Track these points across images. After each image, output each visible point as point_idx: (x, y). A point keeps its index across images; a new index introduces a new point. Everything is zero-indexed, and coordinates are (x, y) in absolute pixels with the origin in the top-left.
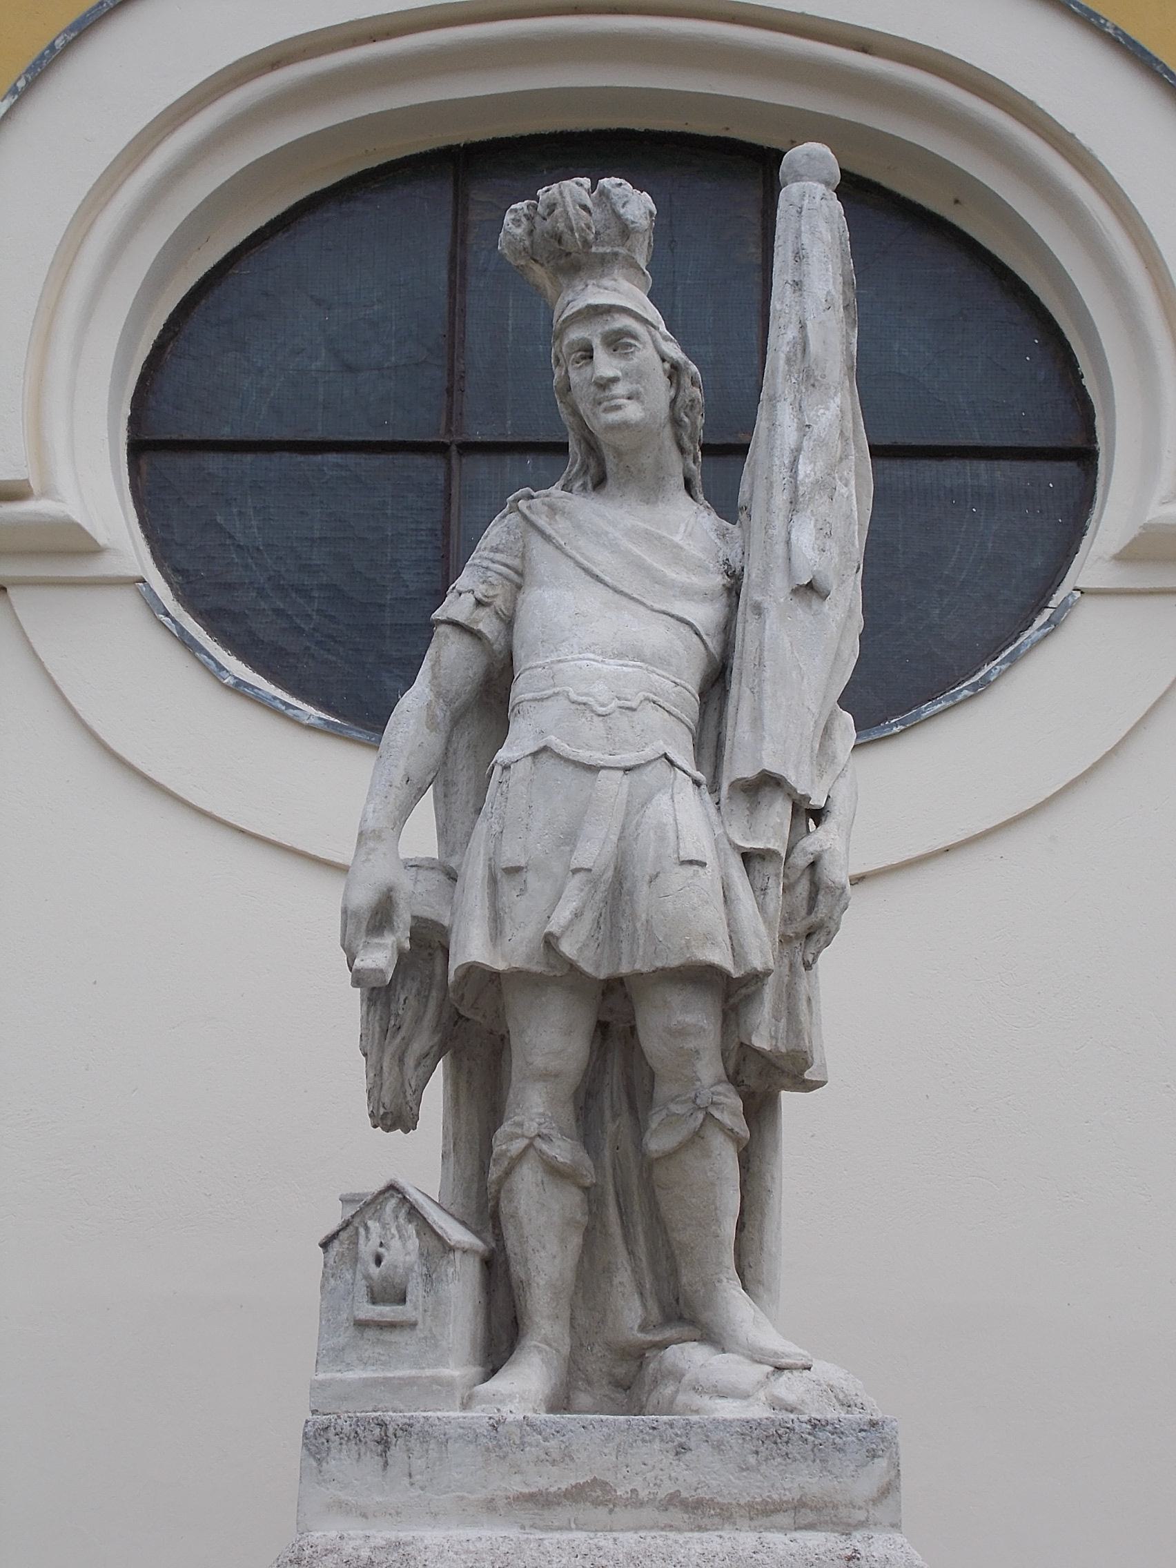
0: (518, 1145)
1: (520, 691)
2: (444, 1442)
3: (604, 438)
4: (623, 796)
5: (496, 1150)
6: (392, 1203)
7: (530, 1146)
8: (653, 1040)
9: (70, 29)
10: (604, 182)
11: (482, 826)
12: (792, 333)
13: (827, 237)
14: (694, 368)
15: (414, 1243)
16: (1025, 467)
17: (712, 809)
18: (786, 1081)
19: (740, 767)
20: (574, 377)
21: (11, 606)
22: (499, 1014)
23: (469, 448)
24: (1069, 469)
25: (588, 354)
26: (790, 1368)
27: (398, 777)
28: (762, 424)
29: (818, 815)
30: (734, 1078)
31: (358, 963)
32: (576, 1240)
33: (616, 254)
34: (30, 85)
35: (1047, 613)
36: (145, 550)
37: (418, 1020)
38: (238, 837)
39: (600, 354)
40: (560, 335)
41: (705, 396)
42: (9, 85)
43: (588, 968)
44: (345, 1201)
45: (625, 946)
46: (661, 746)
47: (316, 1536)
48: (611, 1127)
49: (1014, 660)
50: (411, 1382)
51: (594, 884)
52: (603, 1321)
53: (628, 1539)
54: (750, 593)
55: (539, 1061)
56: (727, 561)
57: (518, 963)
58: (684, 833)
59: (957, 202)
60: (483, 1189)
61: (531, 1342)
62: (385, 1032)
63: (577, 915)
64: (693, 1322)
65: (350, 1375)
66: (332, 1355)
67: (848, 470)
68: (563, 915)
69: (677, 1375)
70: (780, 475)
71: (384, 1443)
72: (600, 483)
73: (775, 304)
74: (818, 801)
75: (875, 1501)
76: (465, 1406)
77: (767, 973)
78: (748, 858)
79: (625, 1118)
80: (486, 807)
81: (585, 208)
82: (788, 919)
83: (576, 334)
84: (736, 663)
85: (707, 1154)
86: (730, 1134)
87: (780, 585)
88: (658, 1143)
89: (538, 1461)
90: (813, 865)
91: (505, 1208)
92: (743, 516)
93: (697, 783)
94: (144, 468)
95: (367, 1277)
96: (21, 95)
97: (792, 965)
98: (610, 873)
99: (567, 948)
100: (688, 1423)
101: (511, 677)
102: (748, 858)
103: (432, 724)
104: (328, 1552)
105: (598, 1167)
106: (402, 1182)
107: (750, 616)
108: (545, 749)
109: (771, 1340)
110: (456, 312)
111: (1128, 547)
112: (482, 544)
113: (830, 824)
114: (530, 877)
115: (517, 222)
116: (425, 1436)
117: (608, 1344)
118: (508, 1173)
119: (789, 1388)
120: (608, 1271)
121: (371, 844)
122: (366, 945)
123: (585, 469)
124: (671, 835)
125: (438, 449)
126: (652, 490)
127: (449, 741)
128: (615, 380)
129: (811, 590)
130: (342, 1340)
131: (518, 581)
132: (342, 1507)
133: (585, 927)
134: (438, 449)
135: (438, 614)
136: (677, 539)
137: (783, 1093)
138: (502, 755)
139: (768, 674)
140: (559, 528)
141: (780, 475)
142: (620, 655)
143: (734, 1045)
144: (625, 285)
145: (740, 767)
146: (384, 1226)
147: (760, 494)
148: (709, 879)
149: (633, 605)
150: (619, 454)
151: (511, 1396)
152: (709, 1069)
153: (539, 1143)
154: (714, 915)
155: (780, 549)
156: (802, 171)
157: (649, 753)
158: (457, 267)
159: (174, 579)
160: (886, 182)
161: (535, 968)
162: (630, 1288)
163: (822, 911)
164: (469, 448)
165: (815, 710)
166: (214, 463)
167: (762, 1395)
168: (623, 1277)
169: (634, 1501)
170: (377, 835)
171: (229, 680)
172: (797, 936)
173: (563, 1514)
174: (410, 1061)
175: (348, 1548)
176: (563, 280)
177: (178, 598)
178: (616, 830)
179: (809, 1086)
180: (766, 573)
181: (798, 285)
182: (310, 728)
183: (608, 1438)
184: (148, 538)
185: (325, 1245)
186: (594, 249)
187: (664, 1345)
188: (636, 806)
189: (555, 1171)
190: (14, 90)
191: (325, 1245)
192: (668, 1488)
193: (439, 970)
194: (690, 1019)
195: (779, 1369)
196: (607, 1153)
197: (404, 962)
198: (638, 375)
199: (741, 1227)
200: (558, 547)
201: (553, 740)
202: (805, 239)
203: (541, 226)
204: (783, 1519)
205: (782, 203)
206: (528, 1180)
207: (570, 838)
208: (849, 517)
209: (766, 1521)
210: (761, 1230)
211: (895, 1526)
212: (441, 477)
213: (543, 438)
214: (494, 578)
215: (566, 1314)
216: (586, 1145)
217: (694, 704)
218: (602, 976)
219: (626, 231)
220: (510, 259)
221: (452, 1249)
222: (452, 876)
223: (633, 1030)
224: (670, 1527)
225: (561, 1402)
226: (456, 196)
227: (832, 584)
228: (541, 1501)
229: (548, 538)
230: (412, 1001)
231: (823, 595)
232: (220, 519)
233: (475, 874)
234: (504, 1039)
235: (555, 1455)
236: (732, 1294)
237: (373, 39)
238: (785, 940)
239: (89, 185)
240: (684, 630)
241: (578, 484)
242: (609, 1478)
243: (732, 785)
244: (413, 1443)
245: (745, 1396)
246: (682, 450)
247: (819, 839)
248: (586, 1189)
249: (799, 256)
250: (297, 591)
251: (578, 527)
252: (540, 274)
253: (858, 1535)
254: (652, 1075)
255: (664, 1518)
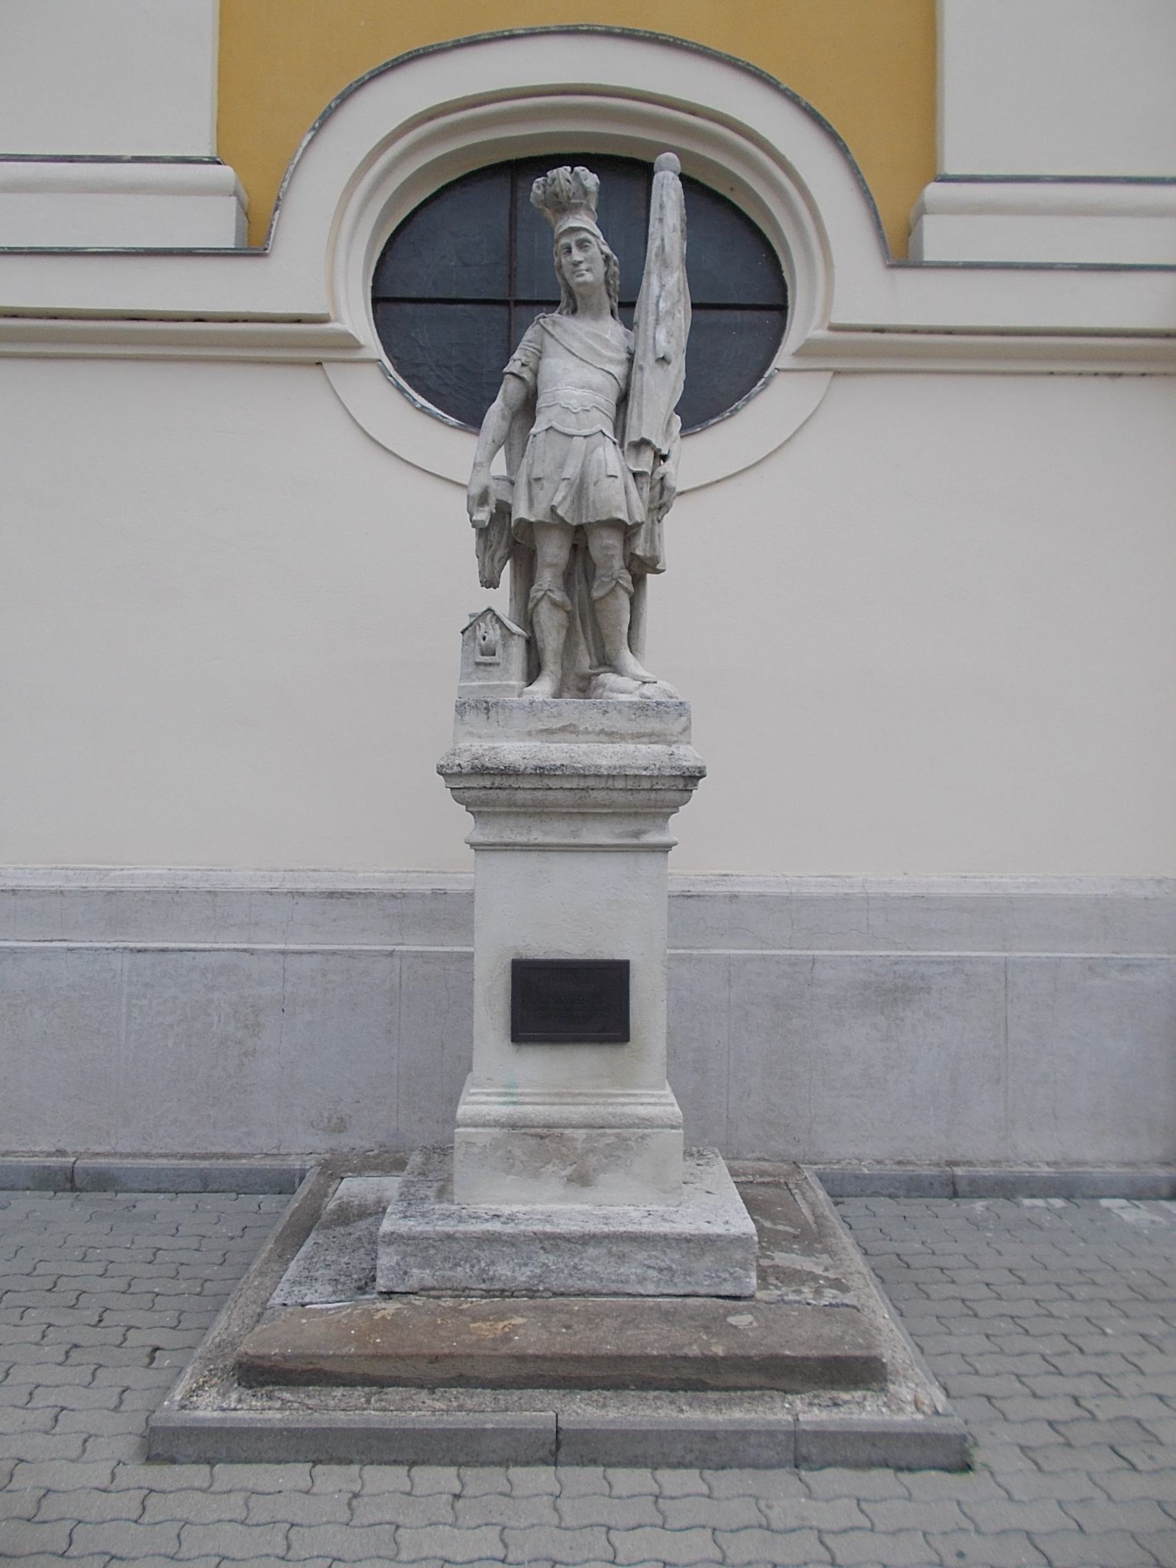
0: (541, 593)
1: (540, 403)
2: (512, 708)
3: (575, 289)
4: (584, 448)
5: (531, 596)
6: (490, 616)
7: (545, 594)
8: (595, 552)
9: (338, 98)
10: (577, 169)
11: (525, 461)
12: (658, 242)
13: (674, 198)
14: (615, 258)
15: (498, 632)
16: (757, 314)
17: (621, 454)
18: (650, 570)
19: (633, 437)
20: (563, 261)
21: (325, 373)
22: (532, 541)
23: (518, 303)
24: (776, 314)
25: (569, 250)
26: (649, 682)
27: (490, 441)
28: (644, 284)
29: (664, 458)
30: (628, 568)
31: (474, 518)
32: (564, 632)
33: (581, 203)
34: (321, 126)
35: (763, 380)
36: (381, 348)
37: (499, 543)
38: (424, 474)
39: (574, 250)
40: (557, 242)
41: (620, 270)
42: (310, 127)
43: (569, 521)
44: (471, 616)
45: (584, 512)
46: (599, 427)
47: (461, 745)
48: (578, 588)
49: (748, 400)
50: (498, 686)
51: (571, 485)
52: (574, 665)
53: (584, 746)
54: (638, 361)
55: (549, 559)
56: (628, 348)
57: (540, 518)
58: (609, 464)
59: (732, 189)
60: (526, 613)
61: (545, 672)
62: (485, 548)
63: (564, 498)
64: (610, 666)
65: (473, 684)
66: (466, 676)
67: (681, 307)
68: (558, 498)
69: (604, 685)
70: (652, 308)
71: (487, 709)
72: (574, 311)
73: (651, 229)
74: (665, 452)
75: (681, 733)
76: (519, 696)
77: (642, 523)
78: (635, 475)
79: (583, 585)
80: (526, 453)
81: (568, 181)
82: (651, 501)
83: (564, 241)
84: (631, 392)
85: (617, 598)
86: (626, 590)
87: (651, 358)
88: (596, 594)
89: (548, 717)
90: (662, 478)
91: (534, 620)
92: (635, 327)
93: (614, 443)
94: (379, 310)
95: (480, 645)
96: (317, 130)
97: (653, 521)
98: (578, 481)
99: (560, 512)
100: (608, 703)
101: (537, 399)
102: (635, 475)
103: (504, 418)
104: (466, 751)
105: (573, 604)
106: (493, 608)
107: (638, 372)
108: (551, 428)
109: (641, 672)
110: (512, 240)
111: (798, 351)
112: (524, 339)
113: (669, 461)
114: (545, 482)
115: (538, 187)
116: (503, 707)
117: (576, 674)
118: (536, 605)
119: (648, 690)
120: (577, 644)
121: (478, 468)
122: (478, 511)
123: (568, 305)
124: (603, 465)
125: (505, 303)
126: (597, 315)
127: (510, 427)
128: (581, 262)
129: (664, 360)
130: (471, 670)
131: (540, 355)
132: (471, 734)
133: (568, 503)
134: (505, 303)
135: (505, 370)
136: (607, 337)
137: (648, 575)
138: (533, 430)
139: (645, 396)
140: (556, 331)
141: (652, 308)
142: (583, 388)
143: (628, 554)
144: (586, 218)
145: (633, 437)
146: (486, 625)
147: (643, 317)
148: (619, 482)
149: (588, 365)
150: (583, 298)
151: (538, 692)
152: (618, 563)
153: (549, 593)
154: (620, 498)
155: (651, 341)
156: (664, 166)
157: (594, 430)
158: (513, 218)
159: (394, 361)
160: (702, 180)
161: (547, 521)
162: (585, 652)
163: (665, 498)
164: (518, 303)
165: (664, 412)
166: (409, 308)
167: (637, 692)
168: (582, 647)
169: (586, 732)
170: (481, 464)
171: (418, 406)
172: (655, 508)
173: (558, 737)
174: (496, 559)
175: (473, 750)
176: (559, 216)
177: (396, 370)
178: (581, 462)
179: (659, 572)
180: (645, 351)
181: (661, 220)
182: (453, 427)
183: (576, 708)
184: (382, 342)
185: (463, 633)
186: (572, 201)
187: (598, 675)
188: (590, 452)
189: (555, 604)
190: (313, 128)
191: (463, 633)
192: (600, 727)
193: (507, 522)
194: (610, 542)
195: (644, 683)
196: (576, 598)
197: (493, 518)
198: (591, 260)
199: (630, 628)
200: (556, 340)
201: (554, 424)
202: (665, 199)
203: (549, 189)
204: (646, 740)
205: (655, 182)
206: (544, 607)
207: (561, 466)
208: (680, 328)
209: (638, 740)
210: (638, 630)
211: (689, 743)
212: (507, 317)
213: (550, 298)
214: (530, 354)
215: (559, 662)
216: (568, 595)
217: (614, 409)
218: (575, 523)
219: (586, 192)
220: (535, 205)
221: (514, 634)
222: (512, 483)
223: (587, 548)
224: (601, 742)
225: (558, 694)
226: (512, 183)
227: (672, 357)
228: (550, 732)
229: (552, 336)
230: (497, 535)
231: (669, 363)
232: (413, 335)
233: (522, 481)
234: (534, 552)
235: (555, 714)
236: (627, 659)
237: (474, 106)
238: (650, 510)
239: (350, 175)
240: (609, 376)
241: (565, 312)
242: (576, 723)
243: (629, 444)
244: (499, 710)
245: (631, 693)
246: (610, 296)
247: (665, 467)
248: (568, 612)
249: (662, 207)
250: (447, 367)
251: (565, 331)
252: (548, 213)
253: (674, 746)
254: (595, 566)
255: (598, 739)
